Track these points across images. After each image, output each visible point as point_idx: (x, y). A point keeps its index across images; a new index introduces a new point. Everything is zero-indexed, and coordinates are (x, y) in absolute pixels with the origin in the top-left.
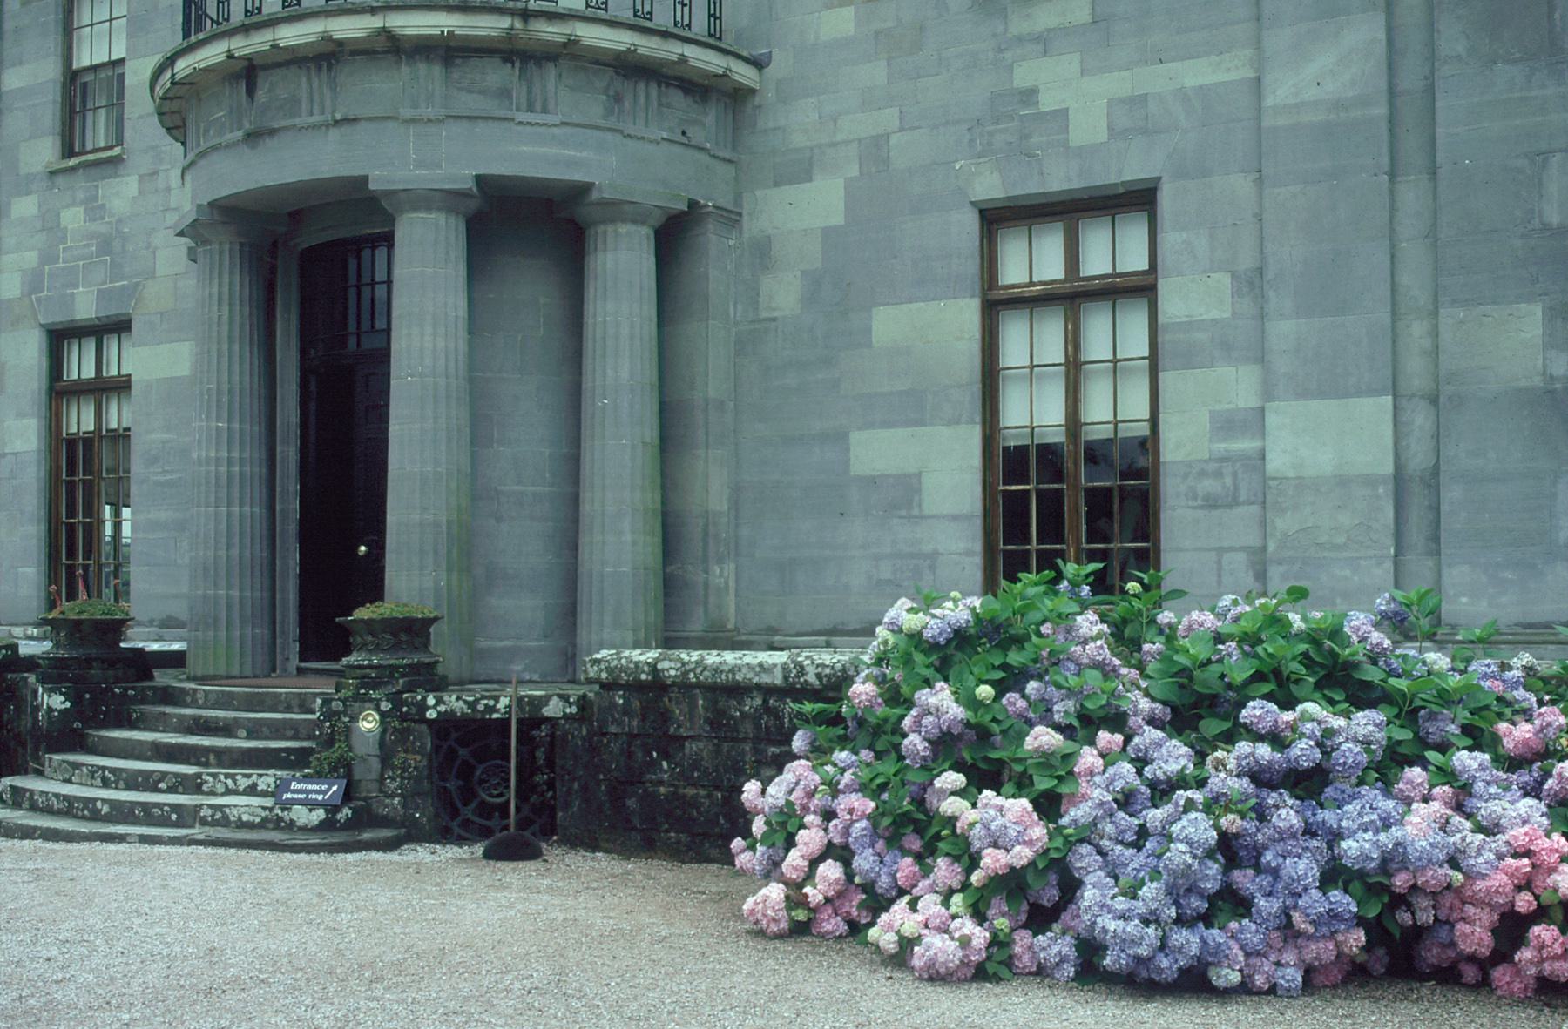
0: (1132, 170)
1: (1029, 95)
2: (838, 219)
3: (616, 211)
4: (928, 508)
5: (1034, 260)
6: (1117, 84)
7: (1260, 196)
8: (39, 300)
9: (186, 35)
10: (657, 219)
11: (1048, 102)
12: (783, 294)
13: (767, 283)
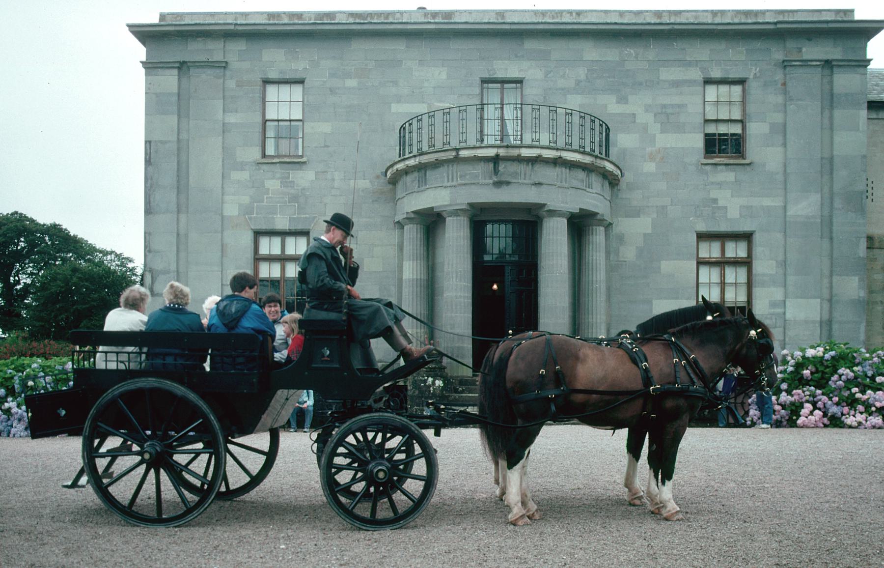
0: (745, 227)
1: (715, 201)
3: (552, 213)
5: (712, 251)
6: (743, 201)
7: (785, 241)
8: (250, 219)
11: (721, 203)
12: (629, 253)
13: (622, 249)
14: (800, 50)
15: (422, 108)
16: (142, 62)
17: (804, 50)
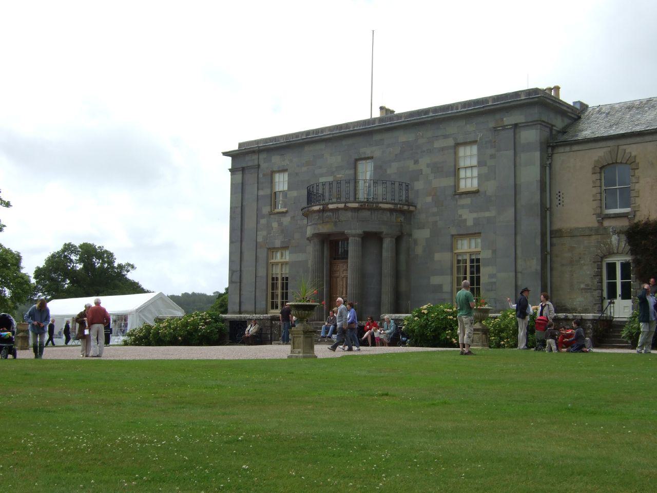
2: (429, 236)
4: (444, 291)
6: (475, 215)
9: (308, 204)
10: (396, 237)
12: (419, 250)
14: (502, 119)
15: (330, 179)
16: (229, 169)
17: (505, 119)
